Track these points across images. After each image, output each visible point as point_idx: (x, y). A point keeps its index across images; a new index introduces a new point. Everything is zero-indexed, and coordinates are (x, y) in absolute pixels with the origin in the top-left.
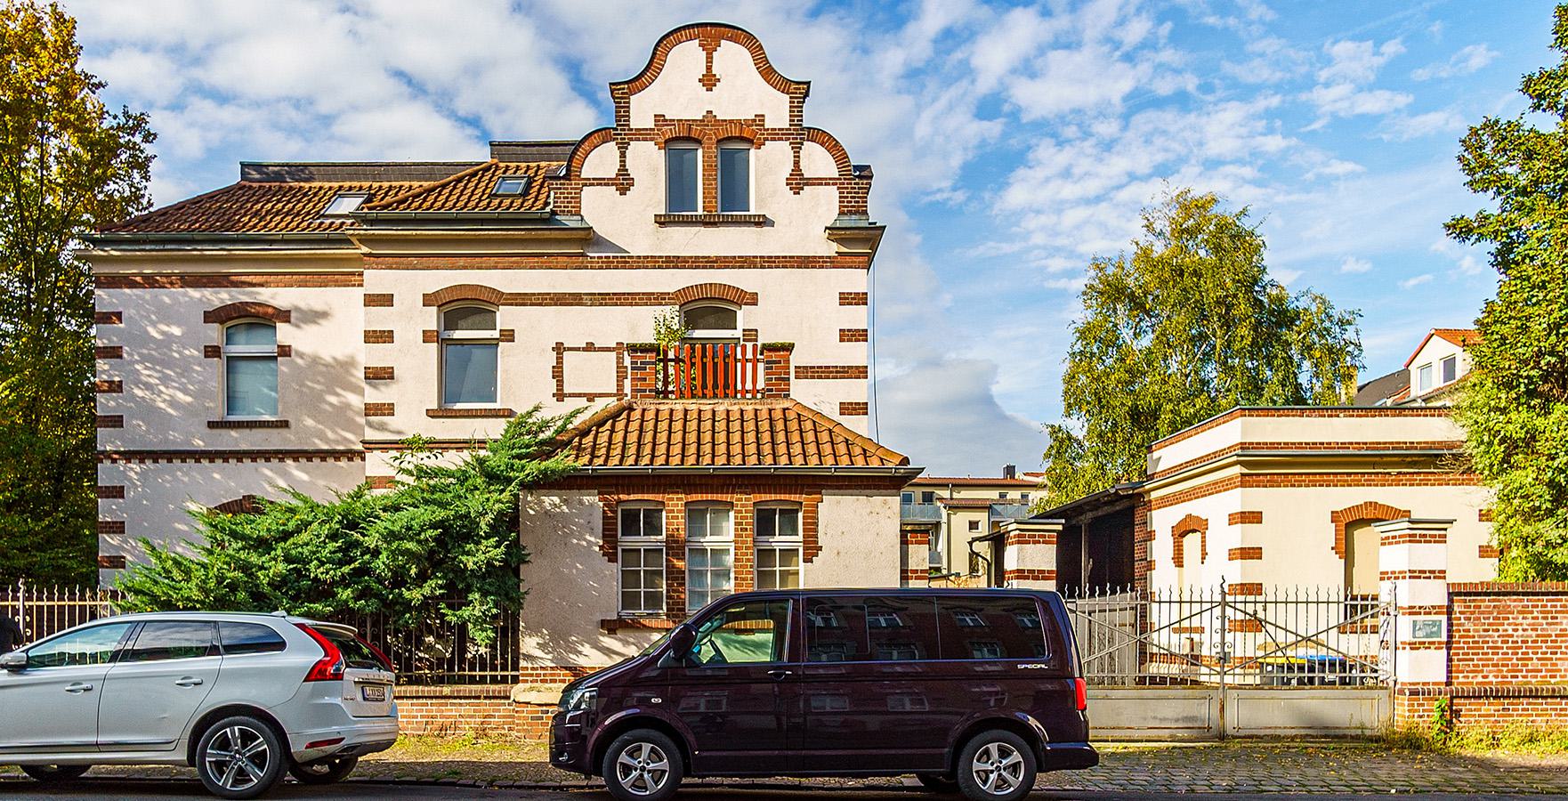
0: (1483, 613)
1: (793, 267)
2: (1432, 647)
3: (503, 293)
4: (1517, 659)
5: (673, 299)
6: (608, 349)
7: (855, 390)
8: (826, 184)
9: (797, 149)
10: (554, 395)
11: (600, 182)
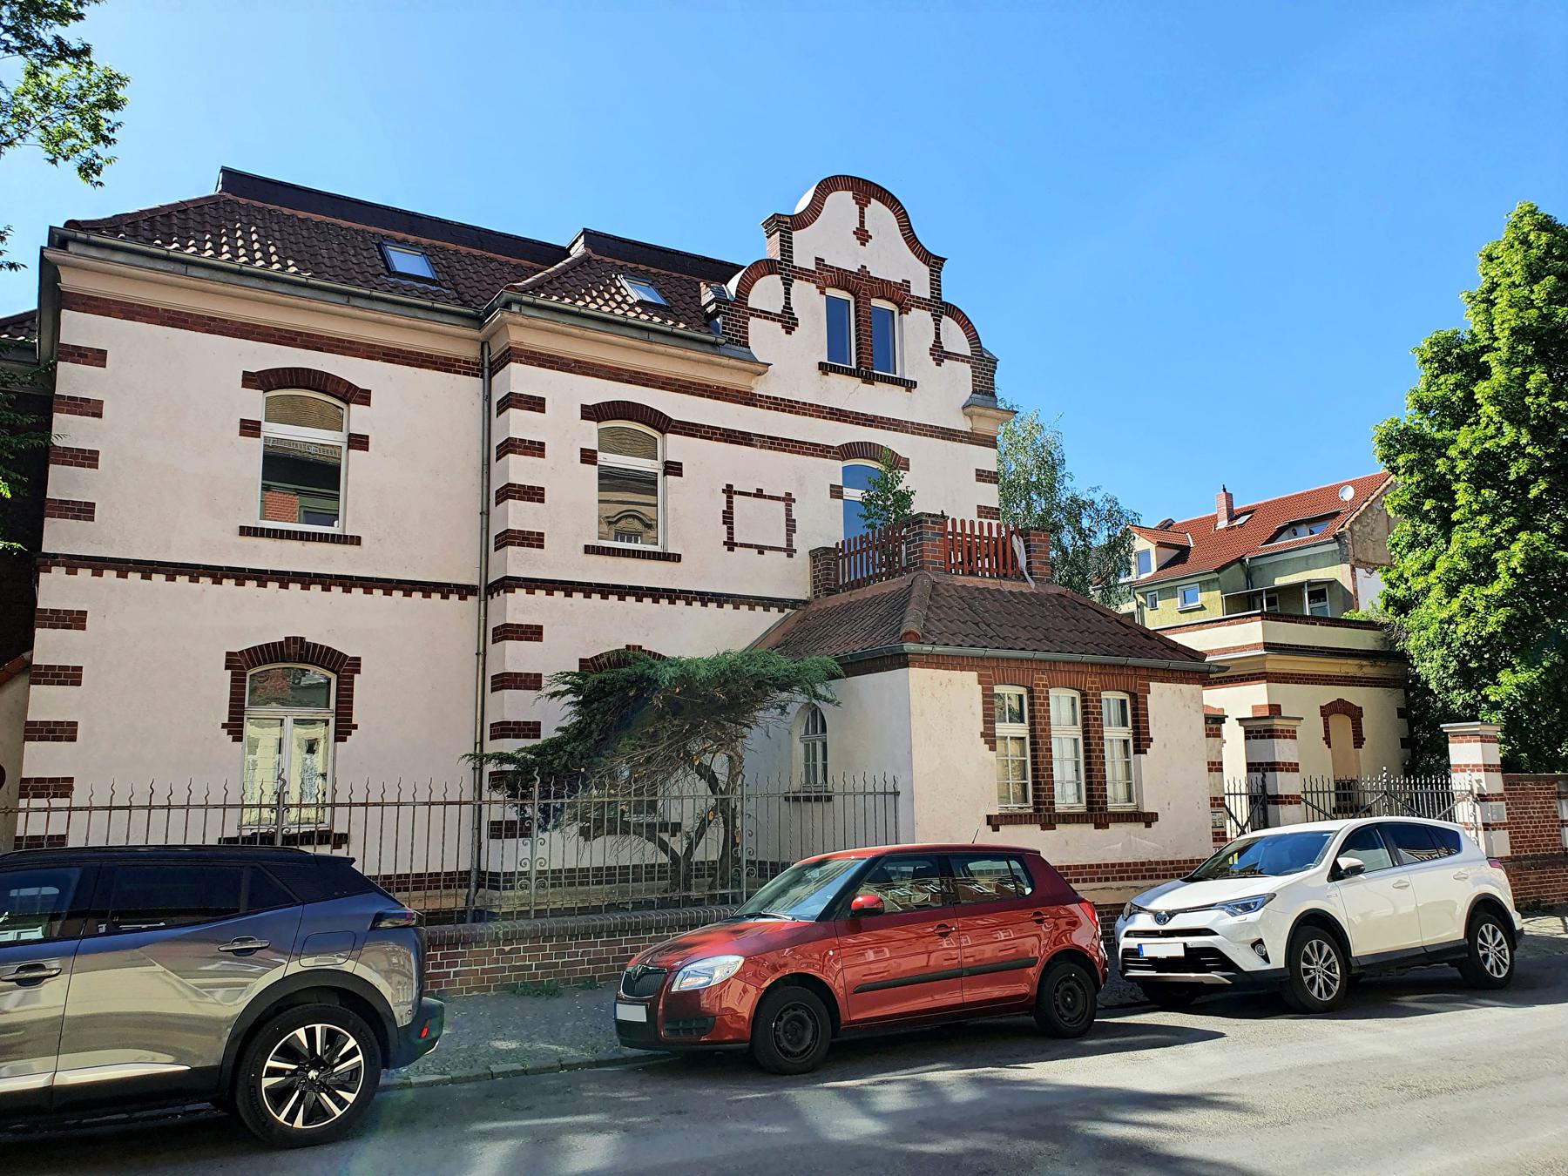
1: (937, 437)
3: (671, 419)
5: (837, 453)
6: (778, 499)
8: (962, 361)
9: (787, 285)
10: (725, 543)
11: (766, 315)
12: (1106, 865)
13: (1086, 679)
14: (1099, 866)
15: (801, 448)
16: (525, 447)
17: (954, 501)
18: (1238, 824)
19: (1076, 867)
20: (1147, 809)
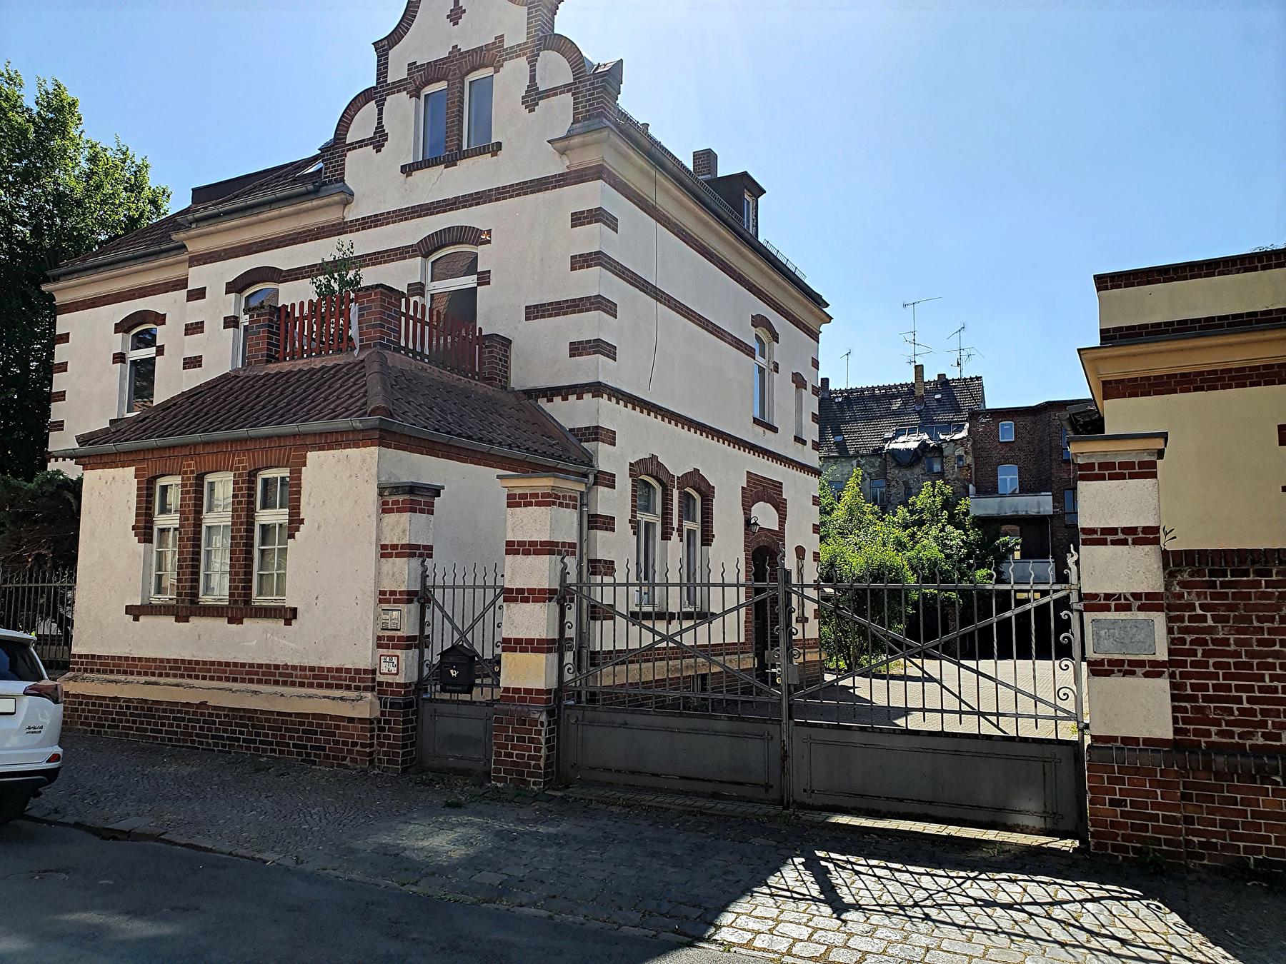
0: (1255, 608)
2: (1139, 671)
4: (1250, 700)
7: (588, 325)
11: (361, 144)
12: (236, 664)
13: (233, 458)
14: (227, 664)
15: (382, 257)
16: (195, 328)
17: (542, 260)
18: (454, 627)
19: (205, 663)
20: (290, 603)
